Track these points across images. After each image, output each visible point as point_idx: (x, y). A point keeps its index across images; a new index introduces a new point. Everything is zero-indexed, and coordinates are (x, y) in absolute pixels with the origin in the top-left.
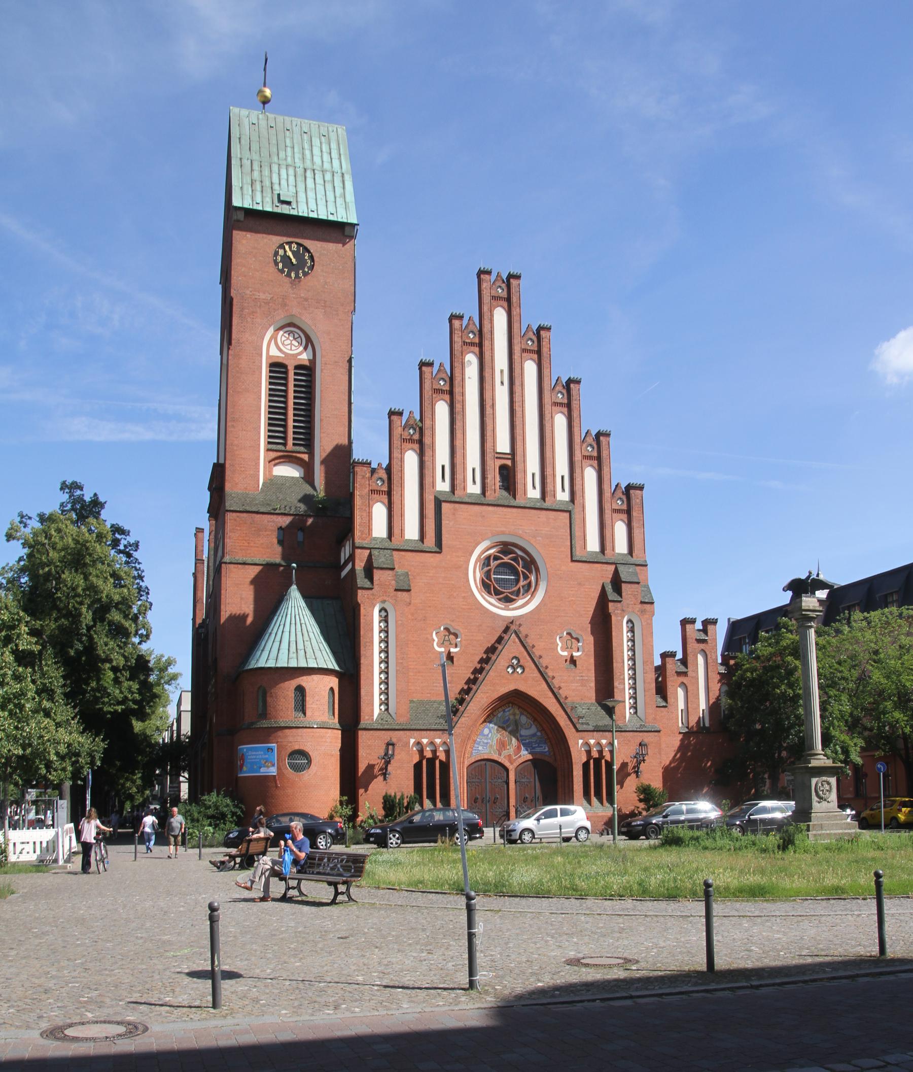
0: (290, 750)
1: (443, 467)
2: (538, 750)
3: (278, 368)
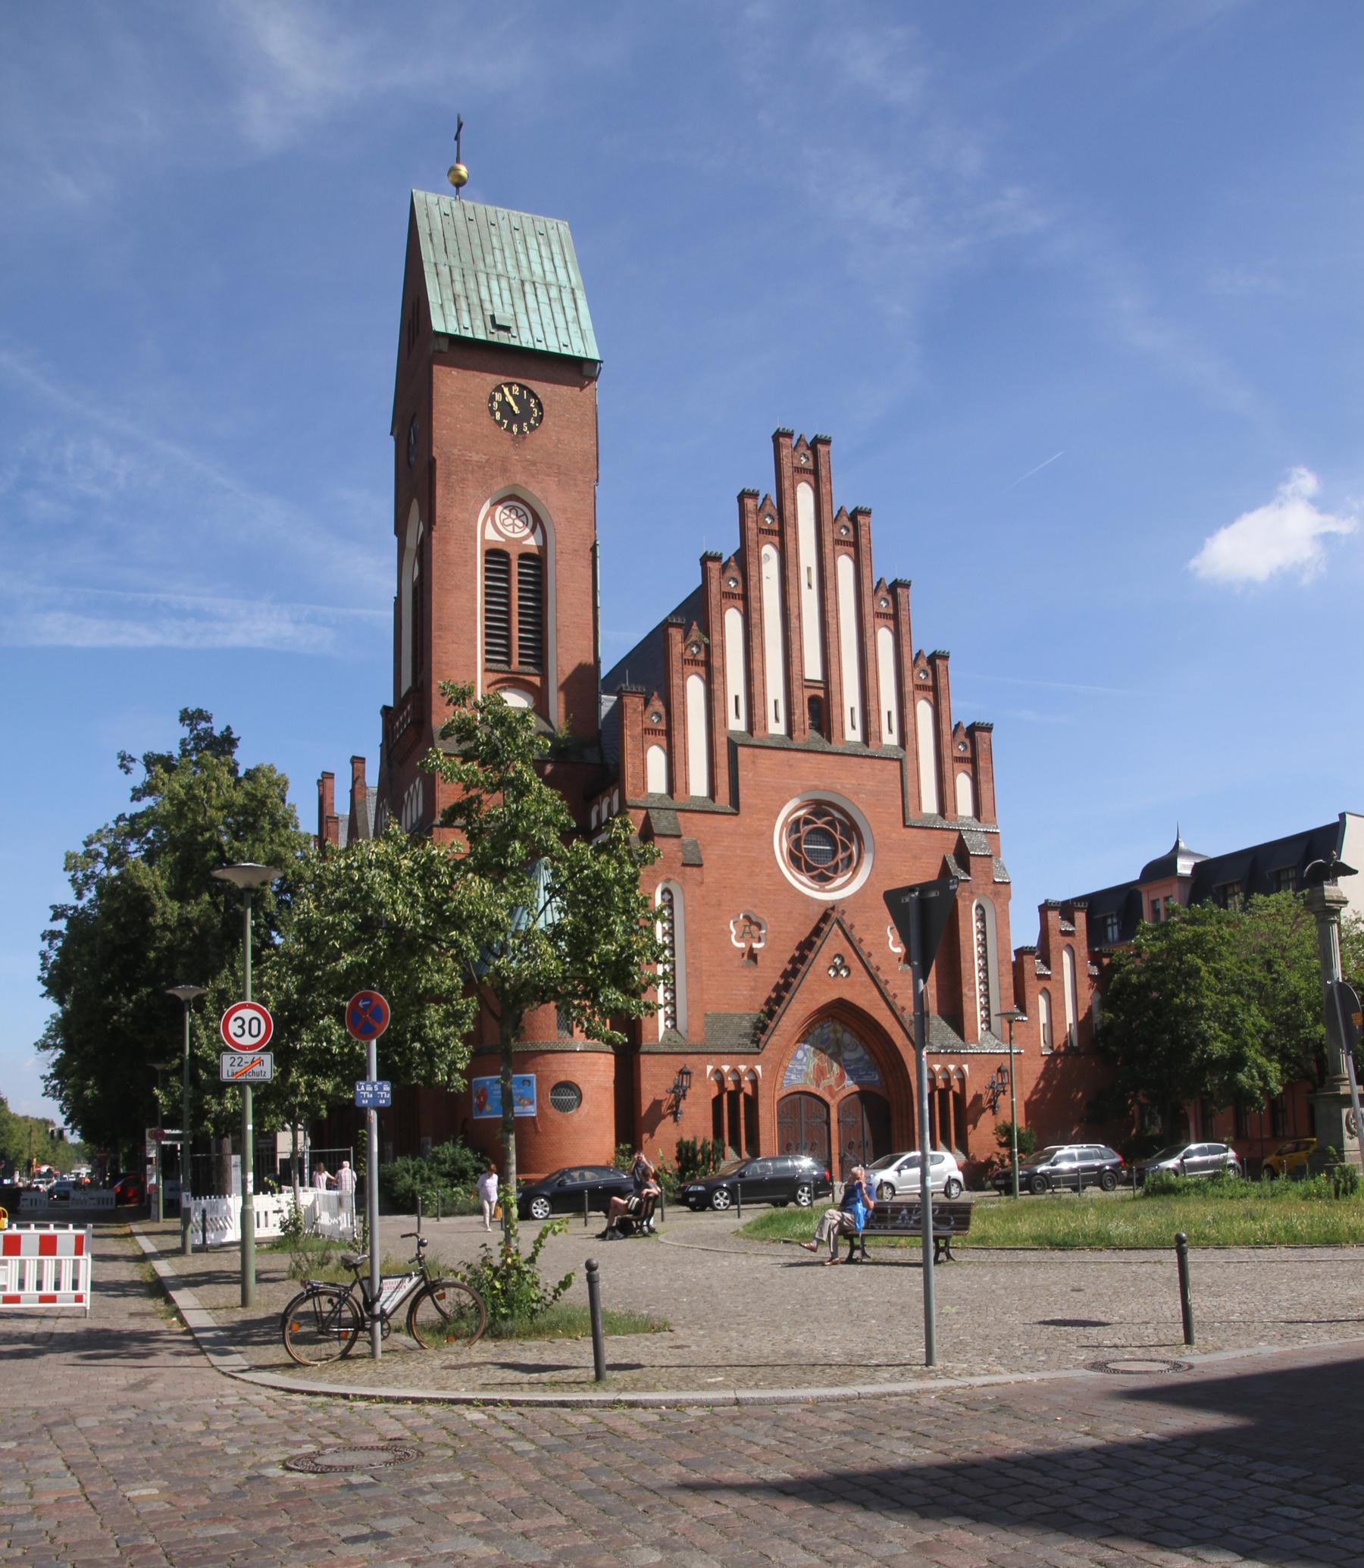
0: (554, 1083)
1: (737, 698)
2: (866, 1078)
3: (496, 556)
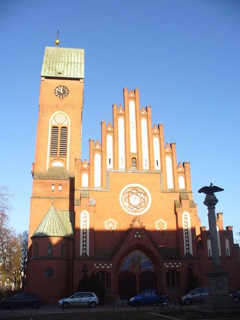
3: (55, 128)
